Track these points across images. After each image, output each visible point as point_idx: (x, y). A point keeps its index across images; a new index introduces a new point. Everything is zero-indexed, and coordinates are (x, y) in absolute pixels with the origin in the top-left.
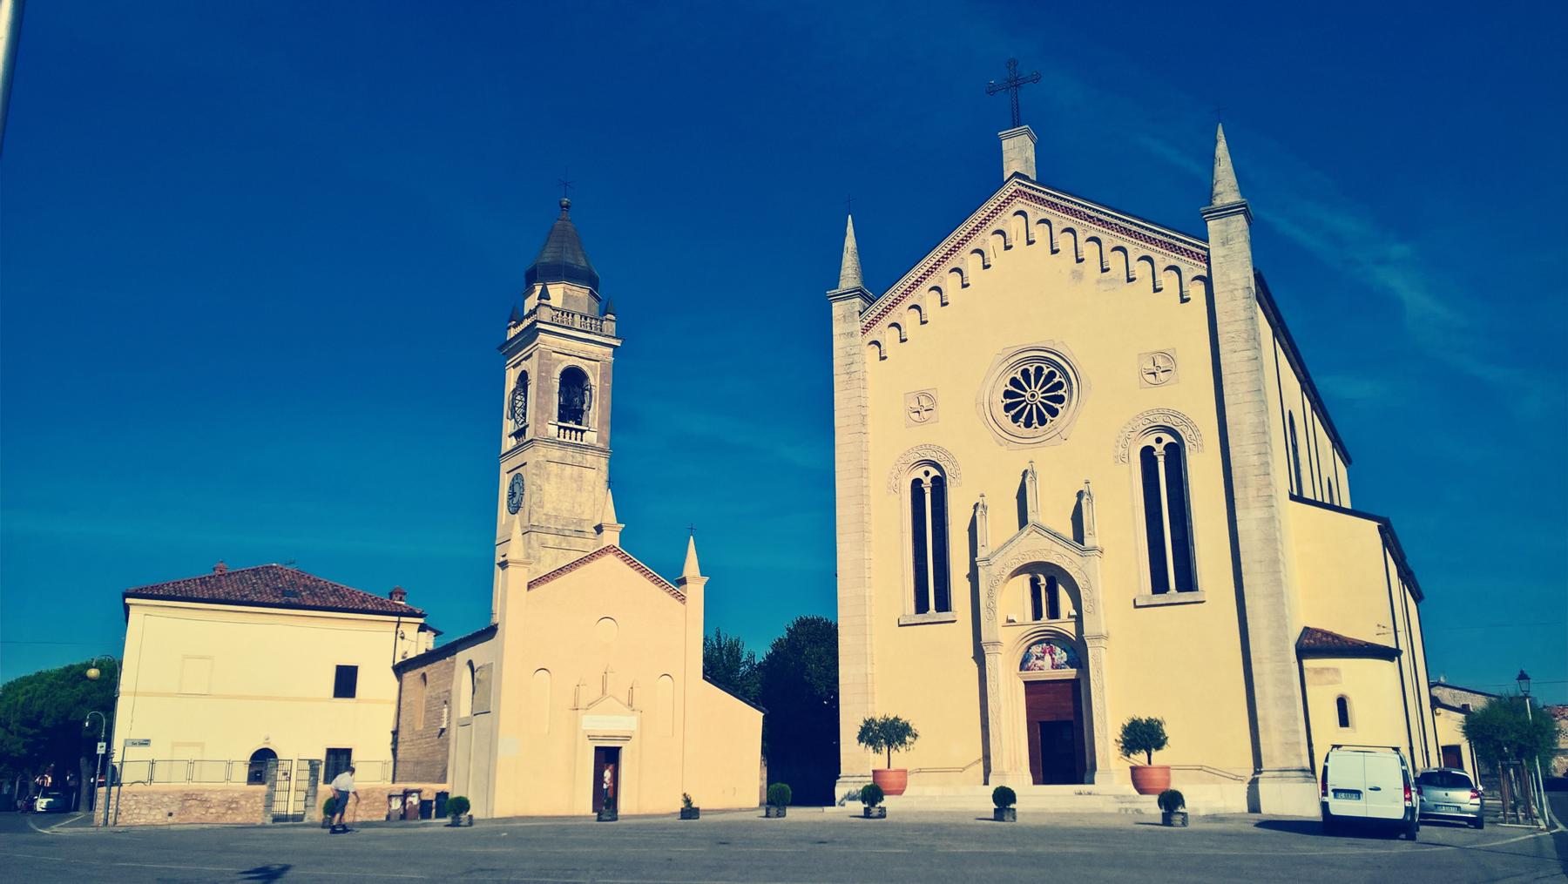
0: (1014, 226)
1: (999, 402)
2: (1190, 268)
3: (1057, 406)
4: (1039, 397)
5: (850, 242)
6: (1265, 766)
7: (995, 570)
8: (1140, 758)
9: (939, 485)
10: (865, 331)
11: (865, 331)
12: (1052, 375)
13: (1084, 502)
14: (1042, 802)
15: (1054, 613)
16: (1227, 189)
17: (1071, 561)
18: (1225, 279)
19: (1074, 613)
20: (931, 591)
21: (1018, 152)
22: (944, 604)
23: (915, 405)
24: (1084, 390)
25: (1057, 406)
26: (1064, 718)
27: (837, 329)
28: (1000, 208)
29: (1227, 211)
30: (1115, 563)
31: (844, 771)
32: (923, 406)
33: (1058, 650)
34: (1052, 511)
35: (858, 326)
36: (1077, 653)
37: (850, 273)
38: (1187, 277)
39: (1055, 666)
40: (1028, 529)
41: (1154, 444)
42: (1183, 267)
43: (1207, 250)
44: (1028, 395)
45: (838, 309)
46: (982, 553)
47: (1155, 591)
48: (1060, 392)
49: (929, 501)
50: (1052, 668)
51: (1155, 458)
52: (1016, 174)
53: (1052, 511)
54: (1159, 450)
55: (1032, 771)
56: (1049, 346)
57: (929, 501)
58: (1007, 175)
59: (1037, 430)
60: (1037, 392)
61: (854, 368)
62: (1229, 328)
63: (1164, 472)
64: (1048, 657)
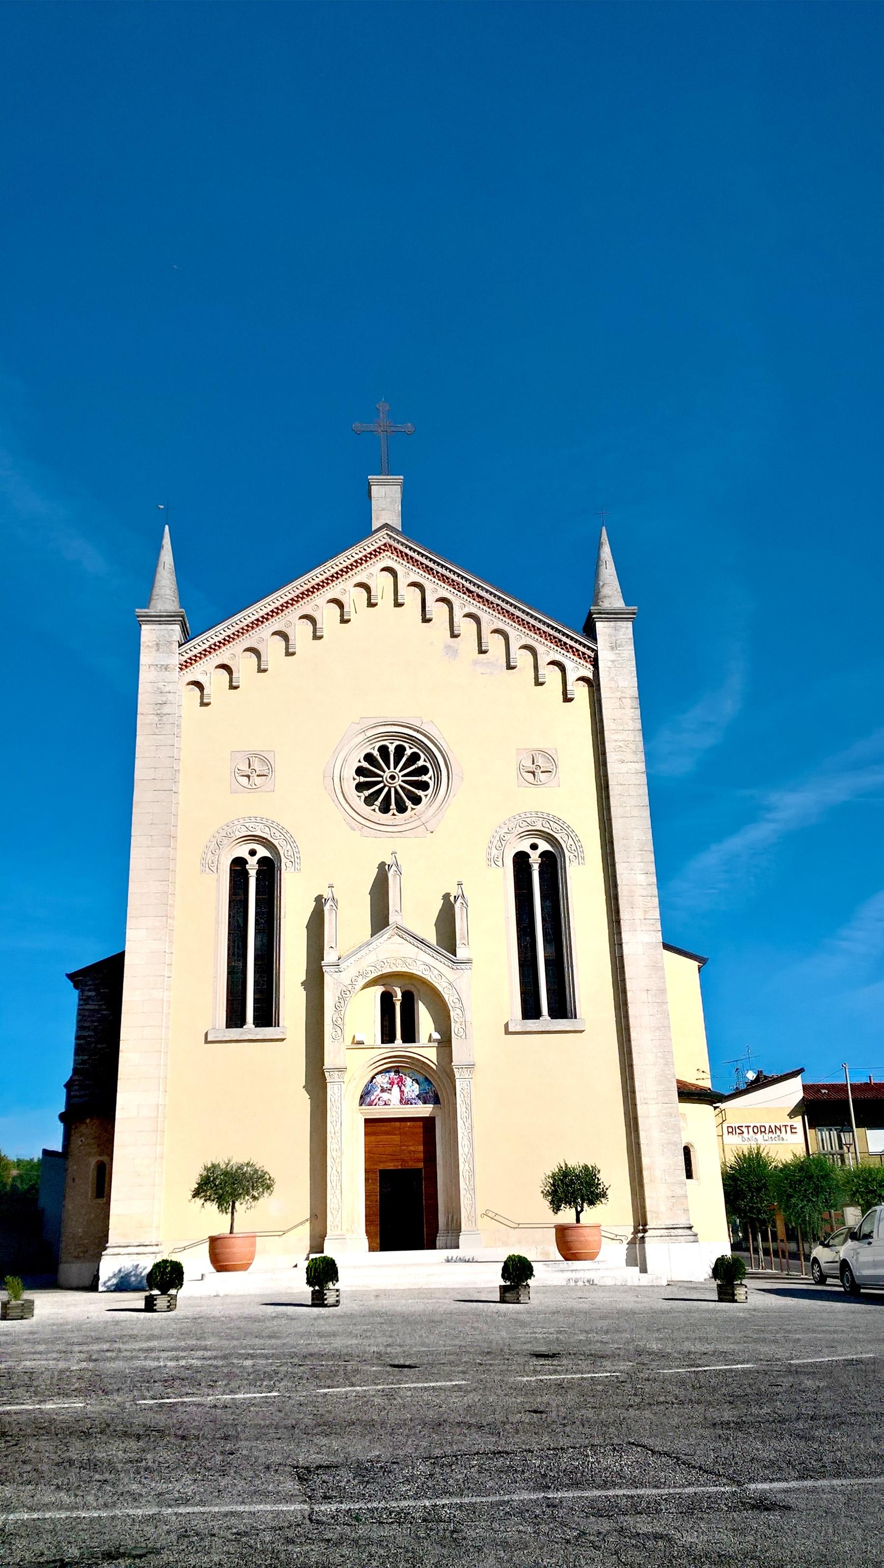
0: (382, 584)
1: (351, 781)
2: (577, 669)
3: (420, 793)
4: (398, 782)
5: (167, 556)
6: (651, 1224)
7: (345, 977)
8: (567, 1215)
9: (269, 870)
10: (184, 666)
11: (184, 666)
12: (415, 757)
13: (327, 908)
14: (372, 1274)
15: (410, 1036)
16: (612, 595)
17: (441, 975)
18: (613, 684)
19: (436, 1036)
20: (250, 998)
21: (386, 501)
22: (266, 1016)
23: (244, 767)
24: (455, 779)
25: (420, 793)
26: (411, 1165)
27: (146, 658)
28: (365, 559)
29: (614, 616)
30: (485, 977)
31: (114, 1237)
32: (255, 769)
33: (409, 1081)
34: (415, 910)
35: (176, 660)
36: (438, 1085)
37: (166, 591)
38: (571, 677)
39: (404, 1101)
40: (388, 932)
41: (528, 850)
42: (569, 665)
43: (595, 652)
44: (387, 774)
45: (148, 633)
46: (329, 956)
47: (229, 1025)
48: (425, 778)
49: (255, 889)
50: (400, 1102)
51: (529, 867)
52: (386, 526)
53: (415, 910)
54: (535, 859)
55: (367, 1232)
56: (416, 723)
57: (255, 889)
58: (375, 525)
59: (393, 818)
60: (398, 775)
61: (166, 709)
62: (616, 737)
63: (538, 884)
64: (396, 1089)
